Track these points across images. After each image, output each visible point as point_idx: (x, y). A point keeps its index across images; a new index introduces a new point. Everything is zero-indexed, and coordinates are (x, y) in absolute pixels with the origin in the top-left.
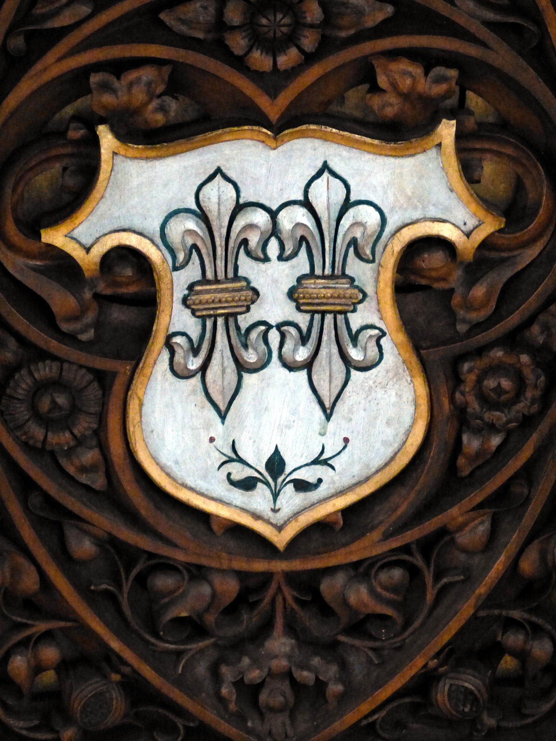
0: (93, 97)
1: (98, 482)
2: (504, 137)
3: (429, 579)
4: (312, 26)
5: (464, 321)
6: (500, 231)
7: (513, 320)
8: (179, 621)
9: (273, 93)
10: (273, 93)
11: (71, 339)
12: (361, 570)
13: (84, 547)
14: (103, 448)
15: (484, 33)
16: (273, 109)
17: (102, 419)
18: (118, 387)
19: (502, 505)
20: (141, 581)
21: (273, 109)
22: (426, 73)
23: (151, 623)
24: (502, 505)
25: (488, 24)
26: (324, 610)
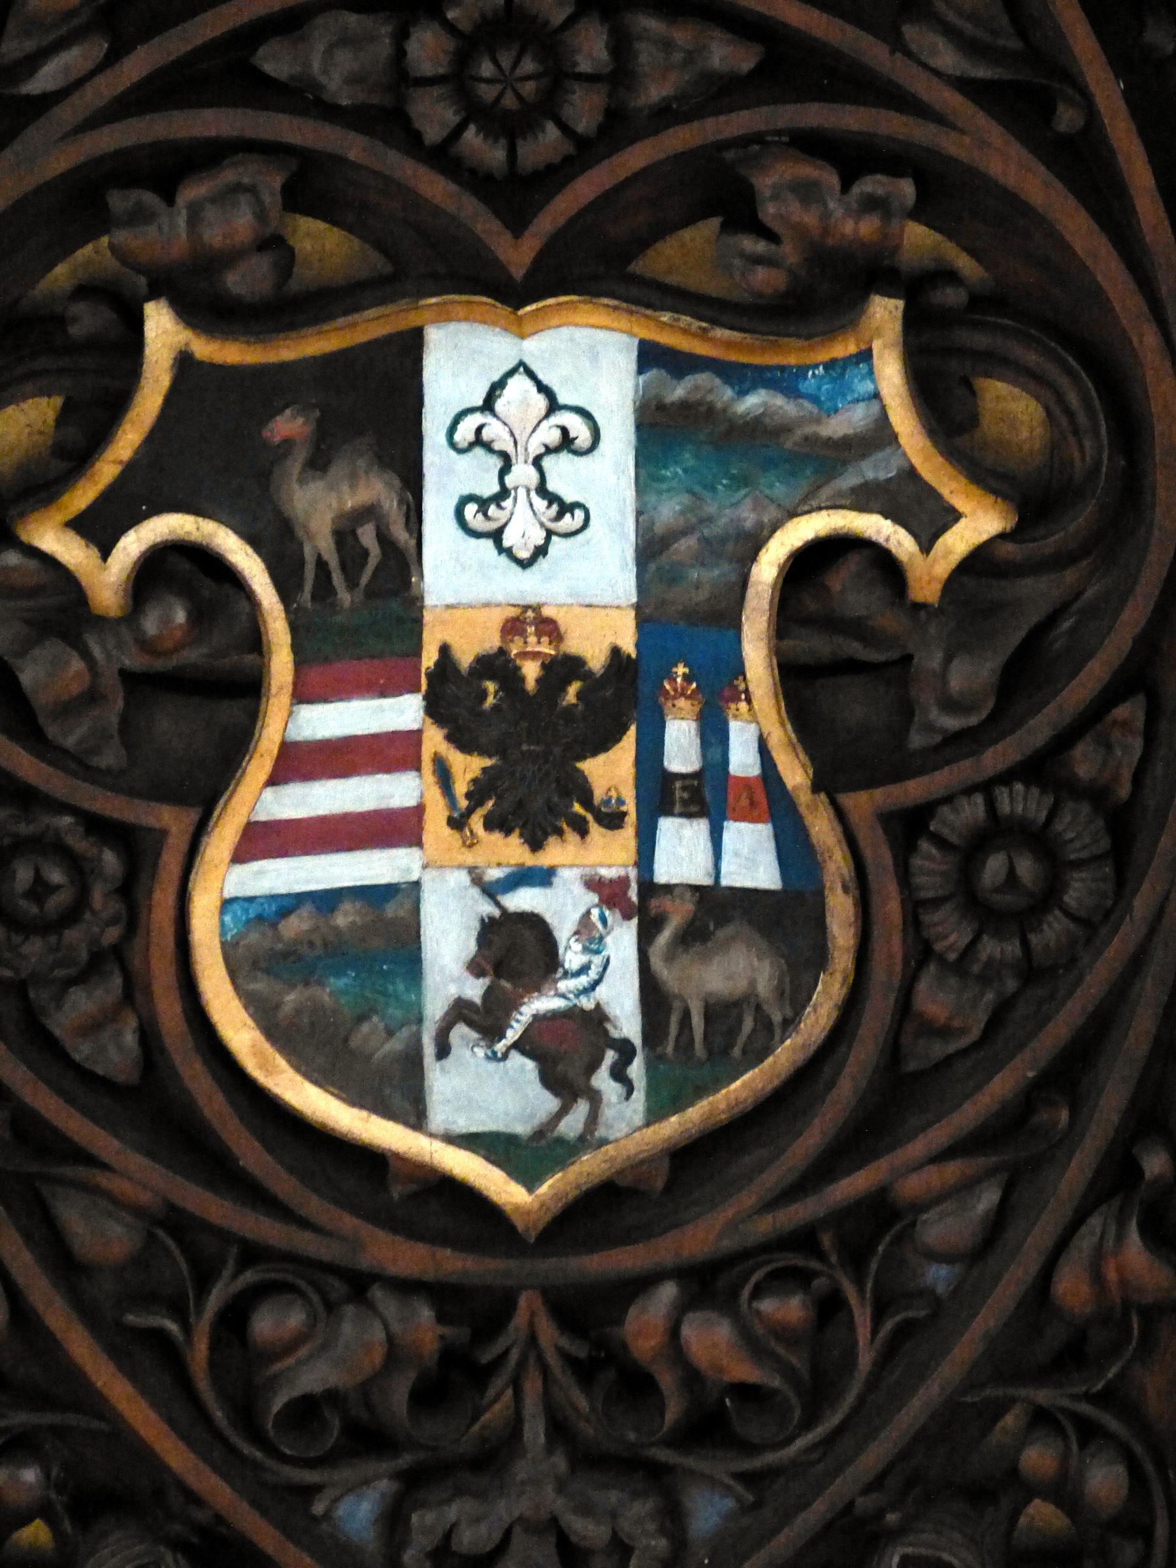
0: (1109, 747)
1: (117, 1053)
2: (1033, 331)
3: (862, 1317)
4: (591, 79)
5: (930, 728)
6: (1002, 536)
7: (1037, 731)
8: (306, 1409)
9: (517, 224)
10: (517, 224)
11: (78, 764)
12: (706, 1284)
13: (102, 1237)
14: (134, 992)
15: (951, 100)
16: (518, 255)
17: (133, 919)
18: (171, 862)
19: (1011, 1143)
20: (234, 1319)
21: (518, 255)
22: (846, 187)
23: (246, 1414)
24: (1011, 1143)
25: (963, 85)
26: (636, 1385)
